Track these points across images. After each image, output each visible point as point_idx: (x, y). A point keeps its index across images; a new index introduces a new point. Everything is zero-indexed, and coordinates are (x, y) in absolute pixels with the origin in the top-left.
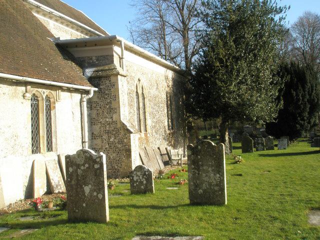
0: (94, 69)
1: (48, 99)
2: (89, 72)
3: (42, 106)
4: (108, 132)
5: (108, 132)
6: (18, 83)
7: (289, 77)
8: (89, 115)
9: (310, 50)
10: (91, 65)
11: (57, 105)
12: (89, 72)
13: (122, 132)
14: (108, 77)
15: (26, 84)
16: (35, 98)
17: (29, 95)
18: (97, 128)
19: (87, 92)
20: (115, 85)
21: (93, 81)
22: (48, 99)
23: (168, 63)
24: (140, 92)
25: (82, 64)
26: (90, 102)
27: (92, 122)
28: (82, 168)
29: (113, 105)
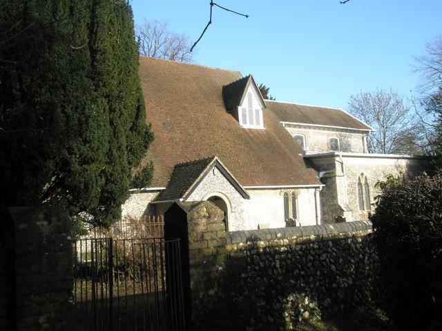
0: (324, 172)
1: (293, 194)
2: (322, 174)
3: (290, 198)
4: (332, 211)
5: (332, 211)
6: (276, 189)
7: (202, 214)
8: (321, 201)
9: (281, 299)
10: (325, 170)
11: (299, 196)
12: (322, 174)
13: (339, 211)
14: (330, 178)
15: (281, 188)
16: (286, 194)
17: (282, 194)
18: (326, 208)
19: (319, 187)
20: (334, 182)
21: (323, 180)
22: (293, 194)
23: (398, 156)
24: (363, 182)
25: (318, 169)
26: (321, 193)
27: (323, 204)
28: (64, 309)
29: (334, 194)
